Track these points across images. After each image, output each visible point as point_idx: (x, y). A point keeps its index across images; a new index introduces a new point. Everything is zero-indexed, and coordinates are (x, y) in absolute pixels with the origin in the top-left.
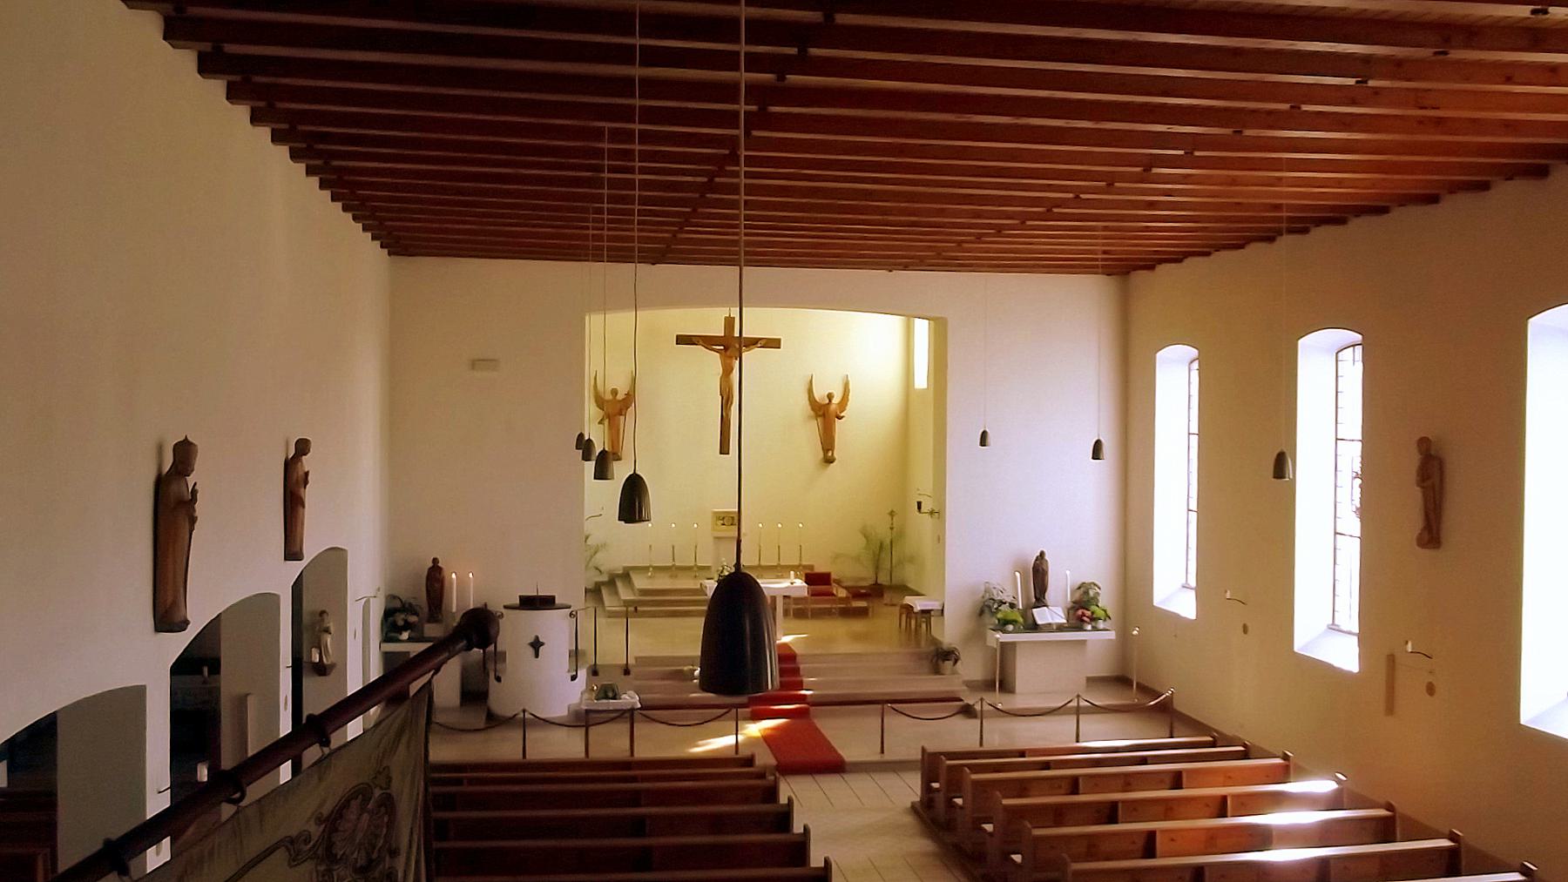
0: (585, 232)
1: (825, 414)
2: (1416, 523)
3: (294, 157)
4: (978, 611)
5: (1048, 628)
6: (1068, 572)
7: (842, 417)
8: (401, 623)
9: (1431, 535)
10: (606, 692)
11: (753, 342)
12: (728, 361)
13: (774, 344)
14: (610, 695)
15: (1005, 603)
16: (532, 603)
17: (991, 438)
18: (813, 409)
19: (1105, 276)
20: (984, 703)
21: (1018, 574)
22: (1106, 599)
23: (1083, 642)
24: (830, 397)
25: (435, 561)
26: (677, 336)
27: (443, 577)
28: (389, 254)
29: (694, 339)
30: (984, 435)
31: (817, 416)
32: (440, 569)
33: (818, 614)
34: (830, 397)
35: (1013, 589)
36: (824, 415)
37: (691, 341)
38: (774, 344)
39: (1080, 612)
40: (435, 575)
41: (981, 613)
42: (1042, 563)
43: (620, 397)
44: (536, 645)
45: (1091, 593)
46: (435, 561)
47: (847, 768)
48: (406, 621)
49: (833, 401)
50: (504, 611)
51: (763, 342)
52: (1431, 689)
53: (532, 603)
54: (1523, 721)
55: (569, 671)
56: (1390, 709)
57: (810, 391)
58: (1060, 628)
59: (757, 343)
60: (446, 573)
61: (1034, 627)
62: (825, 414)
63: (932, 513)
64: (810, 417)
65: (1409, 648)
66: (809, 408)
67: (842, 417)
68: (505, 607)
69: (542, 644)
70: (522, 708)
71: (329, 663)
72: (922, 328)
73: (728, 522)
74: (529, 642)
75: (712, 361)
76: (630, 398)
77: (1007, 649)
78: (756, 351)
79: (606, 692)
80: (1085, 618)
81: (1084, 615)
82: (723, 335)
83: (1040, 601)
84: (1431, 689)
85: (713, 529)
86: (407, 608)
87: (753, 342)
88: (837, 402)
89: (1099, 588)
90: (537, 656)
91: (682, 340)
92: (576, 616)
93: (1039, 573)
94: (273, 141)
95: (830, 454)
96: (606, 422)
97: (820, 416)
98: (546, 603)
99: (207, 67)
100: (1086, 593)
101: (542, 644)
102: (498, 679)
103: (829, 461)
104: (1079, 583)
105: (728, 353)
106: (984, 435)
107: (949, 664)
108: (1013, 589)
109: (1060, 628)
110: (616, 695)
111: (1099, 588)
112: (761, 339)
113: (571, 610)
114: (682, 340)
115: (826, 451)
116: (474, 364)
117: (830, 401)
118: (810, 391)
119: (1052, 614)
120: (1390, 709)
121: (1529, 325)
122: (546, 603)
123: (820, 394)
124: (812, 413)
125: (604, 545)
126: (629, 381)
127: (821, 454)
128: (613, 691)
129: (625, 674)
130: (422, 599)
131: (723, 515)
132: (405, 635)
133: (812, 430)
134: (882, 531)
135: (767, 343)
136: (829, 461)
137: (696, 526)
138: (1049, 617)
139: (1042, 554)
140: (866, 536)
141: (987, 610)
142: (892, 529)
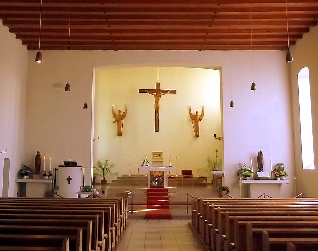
1: (196, 119)
4: (237, 175)
5: (263, 178)
8: (24, 173)
10: (86, 189)
11: (165, 92)
12: (157, 98)
13: (174, 92)
14: (88, 190)
17: (234, 104)
18: (191, 118)
19: (281, 51)
20: (265, 195)
21: (251, 159)
22: (287, 169)
23: (279, 185)
25: (38, 152)
27: (41, 158)
28: (29, 49)
29: (145, 91)
30: (232, 103)
31: (193, 120)
32: (40, 156)
34: (197, 113)
35: (250, 165)
36: (195, 119)
38: (174, 92)
39: (275, 173)
40: (38, 158)
43: (122, 113)
44: (69, 179)
46: (38, 152)
47: (173, 218)
48: (25, 172)
49: (198, 114)
50: (59, 167)
51: (170, 91)
58: (267, 179)
60: (42, 157)
61: (256, 178)
62: (196, 119)
63: (220, 138)
64: (190, 121)
68: (59, 166)
69: (71, 179)
75: (152, 97)
76: (125, 114)
77: (247, 186)
78: (167, 95)
79: (86, 189)
81: (276, 174)
86: (28, 168)
87: (165, 92)
88: (200, 114)
89: (284, 165)
90: (69, 184)
91: (141, 91)
93: (259, 160)
94: (10, 31)
95: (197, 134)
97: (193, 120)
98: (74, 164)
99: (11, 31)
101: (71, 179)
103: (197, 136)
105: (157, 95)
106: (232, 103)
107: (224, 192)
108: (250, 165)
109: (267, 179)
111: (284, 165)
112: (169, 90)
114: (141, 91)
117: (197, 114)
119: (266, 173)
122: (74, 164)
123: (193, 112)
124: (191, 119)
125: (114, 165)
126: (125, 109)
128: (89, 189)
129: (102, 193)
130: (33, 167)
131: (156, 153)
132: (25, 177)
134: (214, 159)
135: (171, 92)
139: (261, 152)
140: (209, 161)
141: (241, 173)
142: (217, 156)
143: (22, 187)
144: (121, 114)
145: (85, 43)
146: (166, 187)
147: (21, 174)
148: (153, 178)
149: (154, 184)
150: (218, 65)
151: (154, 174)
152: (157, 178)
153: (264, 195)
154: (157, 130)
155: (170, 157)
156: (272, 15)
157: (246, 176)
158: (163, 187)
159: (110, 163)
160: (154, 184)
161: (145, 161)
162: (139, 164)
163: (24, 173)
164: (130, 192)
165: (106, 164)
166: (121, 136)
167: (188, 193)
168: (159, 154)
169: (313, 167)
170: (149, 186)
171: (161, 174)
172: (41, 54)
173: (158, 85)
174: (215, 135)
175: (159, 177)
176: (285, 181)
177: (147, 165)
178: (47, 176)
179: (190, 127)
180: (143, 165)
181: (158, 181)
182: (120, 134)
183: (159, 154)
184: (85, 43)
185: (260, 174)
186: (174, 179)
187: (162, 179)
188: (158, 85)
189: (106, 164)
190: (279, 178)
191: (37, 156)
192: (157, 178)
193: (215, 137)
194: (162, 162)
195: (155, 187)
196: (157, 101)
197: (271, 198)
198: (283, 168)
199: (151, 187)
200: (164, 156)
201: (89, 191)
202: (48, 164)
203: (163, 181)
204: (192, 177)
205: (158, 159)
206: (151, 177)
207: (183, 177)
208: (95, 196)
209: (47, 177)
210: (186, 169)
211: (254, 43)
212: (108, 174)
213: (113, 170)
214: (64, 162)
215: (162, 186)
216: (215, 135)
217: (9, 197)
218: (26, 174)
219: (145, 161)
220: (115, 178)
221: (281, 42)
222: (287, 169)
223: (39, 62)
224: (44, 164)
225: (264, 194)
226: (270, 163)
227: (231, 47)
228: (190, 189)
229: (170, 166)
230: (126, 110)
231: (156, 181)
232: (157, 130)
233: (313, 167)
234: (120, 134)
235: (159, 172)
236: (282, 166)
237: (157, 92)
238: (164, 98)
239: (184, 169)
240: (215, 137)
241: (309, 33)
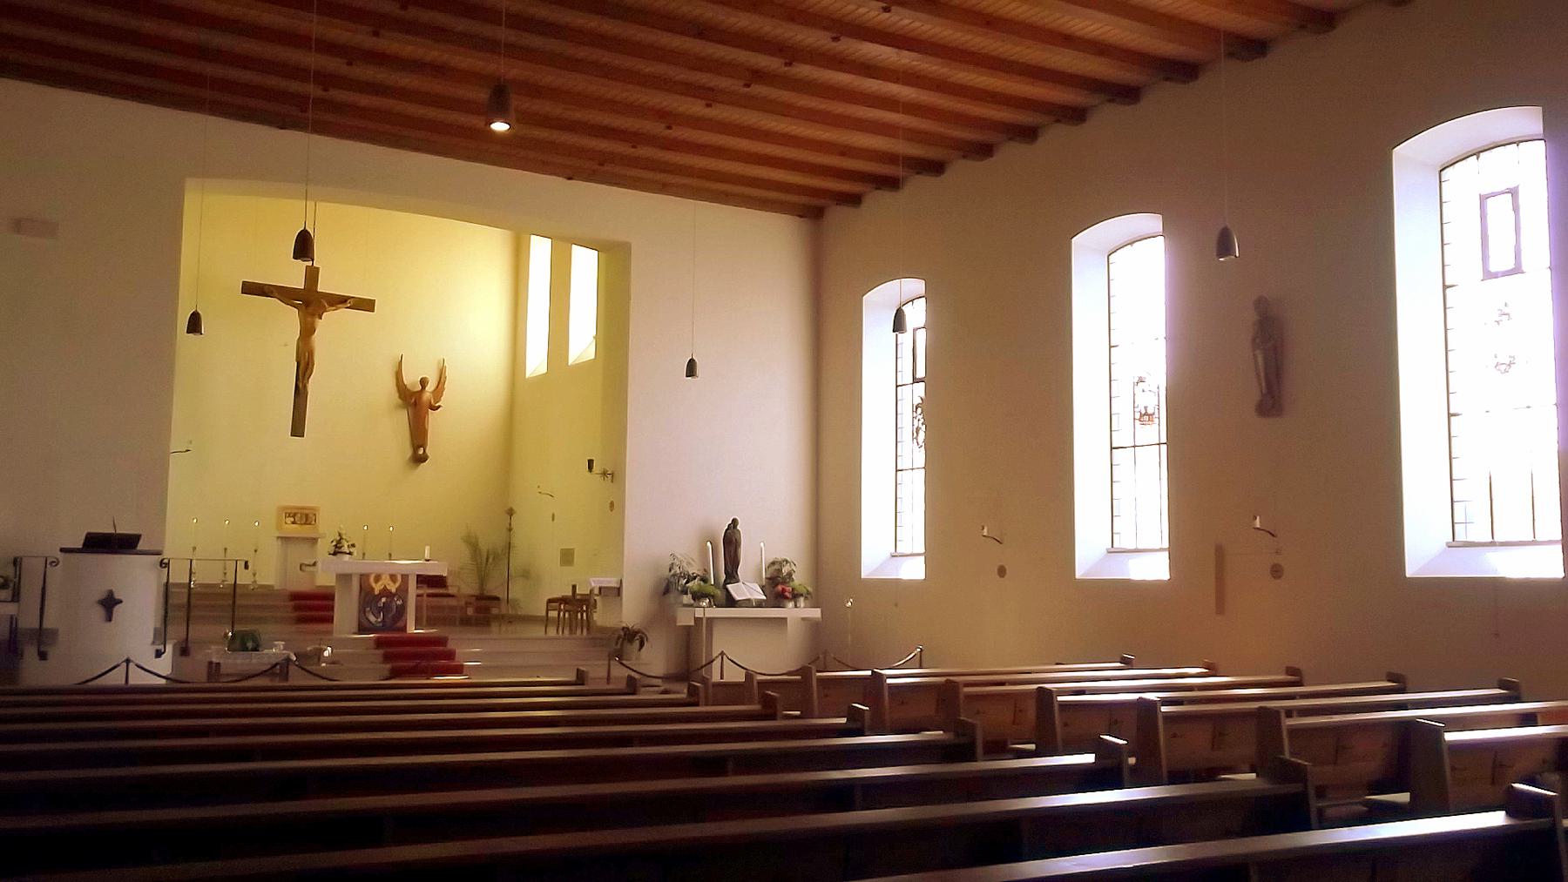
2: (1255, 395)
5: (747, 603)
7: (439, 407)
9: (1271, 402)
12: (309, 319)
13: (367, 305)
14: (250, 645)
15: (695, 578)
16: (100, 544)
19: (798, 218)
20: (725, 657)
22: (800, 579)
24: (423, 382)
26: (242, 293)
34: (423, 382)
38: (367, 305)
41: (667, 591)
42: (735, 533)
44: (109, 603)
45: (785, 570)
50: (60, 555)
52: (1277, 572)
53: (100, 544)
54: (1407, 576)
55: (153, 643)
56: (1220, 608)
57: (399, 375)
58: (760, 604)
59: (346, 301)
61: (731, 602)
65: (1258, 524)
66: (397, 395)
67: (439, 407)
68: (62, 550)
72: (585, 263)
74: (97, 599)
75: (290, 318)
78: (343, 313)
80: (787, 594)
82: (303, 287)
83: (732, 576)
84: (1277, 572)
85: (279, 527)
87: (339, 301)
88: (432, 389)
91: (250, 289)
92: (167, 565)
93: (731, 540)
95: (421, 451)
98: (125, 544)
100: (780, 571)
102: (43, 656)
103: (419, 459)
104: (771, 561)
109: (760, 604)
110: (258, 646)
113: (160, 557)
114: (250, 289)
115: (416, 447)
116: (18, 225)
118: (399, 375)
119: (747, 588)
120: (1220, 608)
121: (1394, 153)
122: (125, 544)
123: (411, 379)
127: (409, 453)
133: (403, 417)
134: (489, 540)
136: (419, 459)
138: (748, 594)
139: (735, 521)
141: (670, 587)
146: (412, 629)
149: (372, 618)
151: (374, 585)
152: (384, 600)
153: (125, 664)
154: (298, 429)
156: (741, 106)
157: (698, 596)
158: (404, 629)
160: (372, 618)
162: (227, 547)
164: (329, 649)
168: (307, 515)
171: (397, 585)
172: (982, 160)
174: (591, 462)
176: (797, 613)
177: (350, 553)
181: (386, 608)
183: (307, 515)
187: (399, 603)
192: (384, 600)
193: (590, 468)
196: (307, 332)
198: (790, 574)
201: (255, 649)
203: (402, 611)
205: (304, 531)
206: (363, 594)
208: (214, 669)
214: (140, 536)
215: (400, 624)
216: (591, 462)
225: (128, 661)
226: (760, 553)
228: (483, 636)
229: (427, 557)
231: (380, 610)
232: (298, 429)
233: (914, 570)
235: (393, 578)
236: (785, 570)
238: (331, 323)
240: (590, 468)
241: (943, 176)
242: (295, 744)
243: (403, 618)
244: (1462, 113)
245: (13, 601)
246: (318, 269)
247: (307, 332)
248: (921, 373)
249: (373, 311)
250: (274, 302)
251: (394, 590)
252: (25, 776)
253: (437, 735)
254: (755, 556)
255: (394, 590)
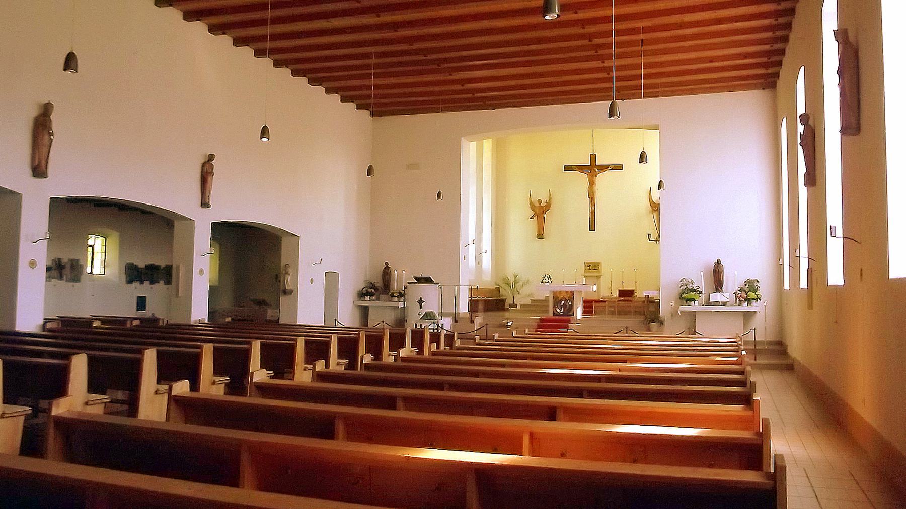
0: (378, 71)
3: (257, 55)
5: (717, 303)
6: (736, 273)
11: (604, 168)
12: (591, 178)
13: (619, 167)
22: (765, 290)
25: (387, 264)
30: (439, 193)
33: (622, 313)
35: (700, 281)
37: (571, 168)
38: (619, 167)
40: (386, 273)
46: (387, 264)
48: (367, 291)
58: (724, 304)
68: (408, 283)
70: (382, 320)
71: (289, 288)
73: (593, 268)
75: (584, 178)
78: (608, 173)
86: (373, 286)
87: (604, 168)
91: (568, 168)
96: (535, 218)
97: (655, 210)
98: (428, 281)
106: (439, 193)
108: (700, 281)
109: (724, 304)
114: (568, 168)
122: (428, 281)
124: (651, 209)
125: (529, 282)
130: (379, 284)
132: (368, 298)
137: (575, 270)
139: (719, 261)
141: (686, 295)
143: (365, 310)
144: (541, 205)
145: (437, 102)
147: (362, 295)
148: (557, 302)
149: (558, 310)
150: (653, 123)
151: (558, 296)
152: (563, 302)
153: (486, 326)
154: (592, 227)
155: (612, 270)
159: (368, 279)
160: (558, 310)
161: (545, 276)
163: (365, 292)
165: (516, 282)
166: (542, 238)
167: (488, 323)
168: (595, 266)
169: (841, 282)
170: (551, 314)
173: (593, 157)
175: (566, 300)
177: (548, 282)
178: (395, 297)
179: (648, 225)
180: (542, 283)
182: (540, 236)
183: (595, 266)
184: (437, 102)
185: (716, 297)
186: (603, 304)
188: (593, 157)
189: (516, 282)
190: (746, 303)
191: (385, 268)
192: (563, 302)
194: (599, 277)
195: (559, 315)
196: (592, 184)
197: (578, 334)
199: (554, 314)
200: (605, 270)
202: (400, 279)
204: (631, 301)
205: (67, 272)
207: (618, 301)
209: (396, 299)
210: (624, 289)
211: (647, 87)
212: (519, 296)
213: (524, 291)
215: (571, 313)
217: (298, 323)
218: (368, 294)
219: (545, 276)
220: (528, 302)
221: (757, 75)
222: (765, 290)
223: (264, 140)
224: (394, 280)
227: (710, 88)
230: (550, 199)
232: (592, 227)
234: (540, 236)
237: (592, 169)
238: (604, 179)
239: (621, 289)
242: (485, 362)
243: (572, 310)
244: (820, 24)
245: (591, 302)
246: (595, 155)
247: (592, 184)
248: (90, 249)
249: (212, 223)
250: (577, 173)
251: (567, 299)
252: (230, 345)
253: (700, 376)
254: (733, 280)
255: (567, 299)
